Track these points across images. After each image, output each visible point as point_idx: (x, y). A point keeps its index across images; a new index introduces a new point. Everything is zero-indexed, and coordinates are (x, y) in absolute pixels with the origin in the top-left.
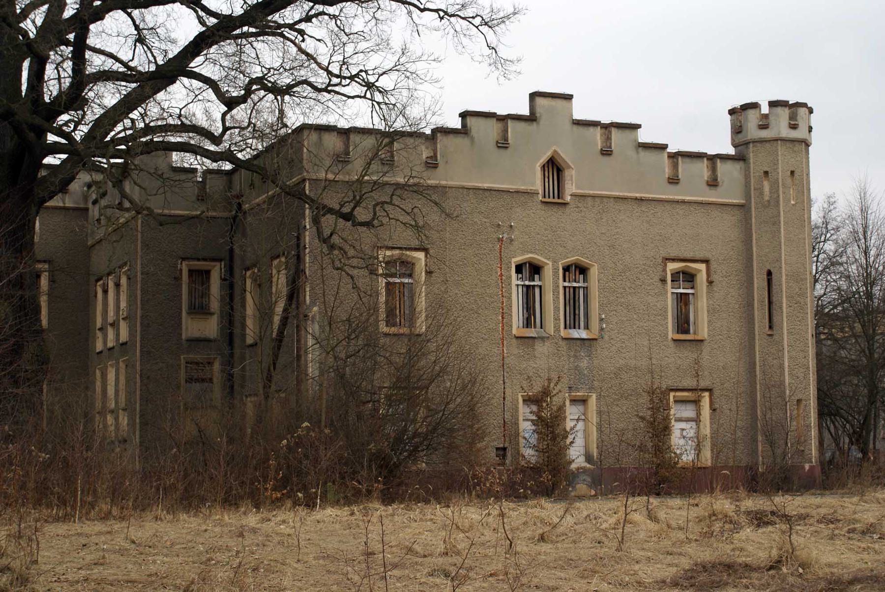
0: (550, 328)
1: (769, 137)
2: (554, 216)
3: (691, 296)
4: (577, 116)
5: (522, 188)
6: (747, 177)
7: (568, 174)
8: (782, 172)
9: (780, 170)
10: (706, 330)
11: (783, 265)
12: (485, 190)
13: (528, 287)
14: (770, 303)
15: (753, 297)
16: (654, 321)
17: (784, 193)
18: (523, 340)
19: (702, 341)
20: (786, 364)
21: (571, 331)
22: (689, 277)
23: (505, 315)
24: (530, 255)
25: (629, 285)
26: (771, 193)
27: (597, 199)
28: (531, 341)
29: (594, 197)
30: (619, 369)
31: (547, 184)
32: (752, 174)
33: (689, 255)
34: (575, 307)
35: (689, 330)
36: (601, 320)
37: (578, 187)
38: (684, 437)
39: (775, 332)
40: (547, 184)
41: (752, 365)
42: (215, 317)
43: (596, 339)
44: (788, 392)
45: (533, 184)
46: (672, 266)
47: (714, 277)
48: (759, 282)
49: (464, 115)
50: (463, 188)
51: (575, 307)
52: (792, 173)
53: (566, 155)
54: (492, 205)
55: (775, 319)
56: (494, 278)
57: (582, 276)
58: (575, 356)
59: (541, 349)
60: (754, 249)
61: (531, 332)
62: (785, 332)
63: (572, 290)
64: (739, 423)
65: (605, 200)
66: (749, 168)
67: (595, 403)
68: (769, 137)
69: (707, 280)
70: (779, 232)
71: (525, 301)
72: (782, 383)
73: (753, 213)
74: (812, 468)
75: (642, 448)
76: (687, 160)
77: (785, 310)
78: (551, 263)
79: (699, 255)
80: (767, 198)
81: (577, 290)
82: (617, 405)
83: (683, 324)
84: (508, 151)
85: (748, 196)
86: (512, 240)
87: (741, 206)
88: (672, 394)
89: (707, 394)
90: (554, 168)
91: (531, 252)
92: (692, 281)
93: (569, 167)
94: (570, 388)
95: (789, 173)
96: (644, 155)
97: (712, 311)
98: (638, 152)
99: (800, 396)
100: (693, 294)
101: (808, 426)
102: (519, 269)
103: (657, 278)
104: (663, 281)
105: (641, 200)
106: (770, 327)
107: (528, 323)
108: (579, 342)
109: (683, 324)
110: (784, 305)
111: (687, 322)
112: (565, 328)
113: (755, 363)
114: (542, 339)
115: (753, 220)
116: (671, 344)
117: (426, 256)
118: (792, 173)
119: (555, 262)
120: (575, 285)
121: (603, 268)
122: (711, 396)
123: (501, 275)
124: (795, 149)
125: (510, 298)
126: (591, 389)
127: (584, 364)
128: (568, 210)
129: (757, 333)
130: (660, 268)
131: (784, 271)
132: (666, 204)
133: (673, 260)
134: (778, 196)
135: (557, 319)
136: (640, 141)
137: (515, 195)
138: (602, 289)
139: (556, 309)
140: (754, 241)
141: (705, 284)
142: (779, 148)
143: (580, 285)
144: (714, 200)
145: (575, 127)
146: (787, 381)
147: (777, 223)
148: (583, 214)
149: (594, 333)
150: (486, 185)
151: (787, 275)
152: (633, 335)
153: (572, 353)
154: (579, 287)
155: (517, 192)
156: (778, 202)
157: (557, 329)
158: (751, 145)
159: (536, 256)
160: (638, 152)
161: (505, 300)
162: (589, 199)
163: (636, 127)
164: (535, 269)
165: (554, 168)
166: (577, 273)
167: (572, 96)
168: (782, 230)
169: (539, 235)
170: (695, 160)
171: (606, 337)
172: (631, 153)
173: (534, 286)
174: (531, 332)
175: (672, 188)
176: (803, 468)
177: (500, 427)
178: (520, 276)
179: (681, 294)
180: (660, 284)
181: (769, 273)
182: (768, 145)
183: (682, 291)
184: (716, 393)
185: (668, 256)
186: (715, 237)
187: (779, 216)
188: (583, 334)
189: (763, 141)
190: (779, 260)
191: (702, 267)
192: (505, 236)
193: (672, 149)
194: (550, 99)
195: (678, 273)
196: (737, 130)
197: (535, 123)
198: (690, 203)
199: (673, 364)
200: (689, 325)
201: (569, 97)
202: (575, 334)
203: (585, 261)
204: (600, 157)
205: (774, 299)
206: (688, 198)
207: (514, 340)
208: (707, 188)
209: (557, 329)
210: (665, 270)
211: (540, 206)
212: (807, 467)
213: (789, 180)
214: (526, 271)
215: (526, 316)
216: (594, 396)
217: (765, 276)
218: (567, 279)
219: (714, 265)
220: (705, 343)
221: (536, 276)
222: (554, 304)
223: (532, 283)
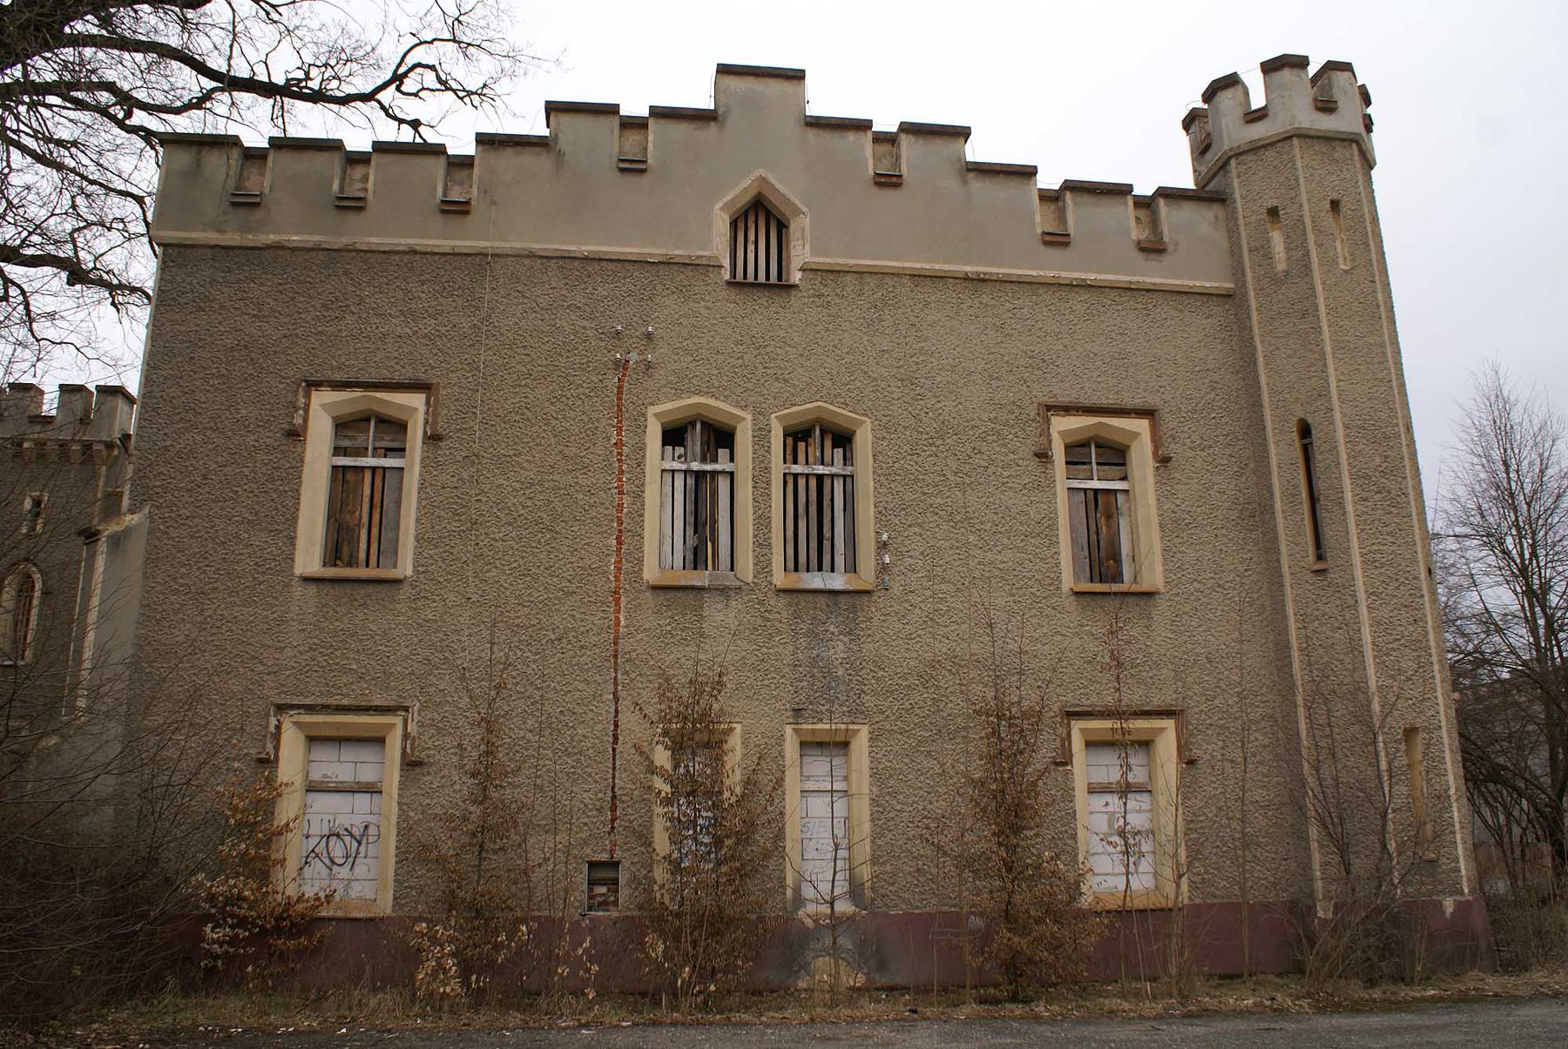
0: (747, 567)
1: (1288, 150)
2: (760, 313)
3: (1121, 498)
4: (813, 110)
5: (678, 252)
6: (1233, 233)
7: (800, 228)
8: (1308, 203)
9: (1304, 198)
10: (1159, 569)
11: (1336, 403)
12: (587, 259)
13: (699, 476)
14: (1313, 500)
15: (1270, 487)
16: (1022, 550)
17: (1319, 245)
18: (671, 594)
19: (1150, 594)
20: (1367, 636)
21: (804, 575)
22: (1115, 455)
23: (627, 536)
24: (702, 400)
26: (1288, 250)
27: (868, 279)
28: (691, 597)
29: (860, 273)
30: (934, 664)
31: (740, 254)
32: (1241, 222)
33: (1108, 400)
34: (816, 521)
35: (1121, 574)
36: (883, 546)
37: (816, 251)
39: (1330, 563)
40: (740, 254)
41: (1283, 649)
43: (868, 592)
44: (1376, 707)
45: (707, 244)
46: (1063, 425)
47: (1172, 449)
48: (1281, 450)
49: (552, 108)
50: (532, 255)
51: (816, 521)
52: (1335, 205)
53: (787, 187)
54: (602, 291)
55: (1328, 532)
57: (839, 452)
58: (812, 634)
59: (717, 614)
60: (1263, 379)
61: (701, 578)
62: (1357, 560)
63: (813, 482)
64: (1258, 794)
65: (888, 279)
66: (1234, 211)
67: (866, 750)
68: (1288, 150)
69: (1155, 454)
70: (1317, 329)
71: (690, 507)
72: (1360, 686)
73: (1253, 304)
74: (1459, 906)
75: (967, 863)
76: (1087, 199)
77: (1350, 508)
78: (749, 417)
79: (406, 374)
80: (1281, 267)
81: (827, 482)
83: (1103, 560)
84: (645, 180)
85: (1238, 272)
86: (649, 366)
87: (1227, 296)
88: (1077, 726)
89: (1169, 724)
90: (761, 216)
91: (699, 393)
92: (1124, 464)
93: (798, 212)
96: (977, 184)
97: (1171, 526)
98: (965, 183)
99: (1410, 720)
100: (1127, 491)
101: (1442, 797)
102: (673, 436)
103: (1026, 450)
104: (1043, 456)
105: (981, 280)
106: (1320, 558)
107: (697, 559)
109: (1103, 560)
110: (1348, 496)
111: (1115, 556)
112: (796, 569)
113: (1288, 647)
114: (724, 591)
115: (1255, 316)
116: (1071, 603)
117: (428, 403)
118: (1335, 205)
119: (760, 414)
120: (820, 470)
121: (885, 429)
123: (619, 444)
125: (639, 496)
126: (857, 713)
127: (837, 651)
128: (795, 300)
129: (1286, 570)
130: (1033, 428)
131: (1338, 416)
132: (1041, 290)
133: (1067, 410)
134: (1307, 254)
135: (762, 544)
136: (970, 158)
137: (662, 270)
138: (884, 476)
139: (763, 521)
140: (1261, 360)
141: (1150, 463)
142: (1297, 152)
143: (834, 470)
144: (1158, 280)
145: (811, 133)
146: (1372, 682)
147: (1308, 311)
148: (834, 310)
149: (867, 575)
150: (587, 249)
151: (1347, 427)
152: (969, 577)
153: (804, 627)
154: (832, 476)
155: (668, 263)
156: (1307, 267)
157: (763, 567)
158: (1233, 162)
159: (712, 402)
160: (965, 183)
161: (626, 500)
162: (849, 277)
163: (963, 133)
164: (721, 437)
165: (761, 216)
166: (828, 444)
168: (1324, 324)
169: (761, 374)
170: (1105, 200)
171: (896, 589)
172: (949, 182)
173: (714, 474)
174: (701, 578)
175: (1054, 254)
176: (1439, 906)
178: (679, 450)
180: (1034, 463)
181: (1305, 431)
182: (1270, 154)
183: (1096, 484)
185: (1051, 401)
186: (1169, 361)
187: (1314, 295)
188: (837, 582)
189: (1257, 148)
190: (1324, 393)
191: (1141, 426)
192: (634, 356)
193: (1048, 180)
194: (751, 79)
195: (1084, 444)
196: (1201, 150)
197: (713, 124)
198: (1099, 288)
199: (1060, 643)
200: (1118, 562)
201: (797, 76)
202: (816, 581)
203: (840, 413)
204: (875, 190)
205: (1321, 485)
206: (1091, 277)
208: (1140, 257)
209: (763, 567)
210: (1046, 432)
211: (724, 293)
212: (1449, 905)
213: (1328, 221)
214: (695, 439)
215: (691, 542)
216: (864, 732)
217: (1295, 436)
218: (801, 457)
219: (1169, 423)
220: (1158, 600)
221: (723, 453)
222: (756, 509)
223: (708, 467)
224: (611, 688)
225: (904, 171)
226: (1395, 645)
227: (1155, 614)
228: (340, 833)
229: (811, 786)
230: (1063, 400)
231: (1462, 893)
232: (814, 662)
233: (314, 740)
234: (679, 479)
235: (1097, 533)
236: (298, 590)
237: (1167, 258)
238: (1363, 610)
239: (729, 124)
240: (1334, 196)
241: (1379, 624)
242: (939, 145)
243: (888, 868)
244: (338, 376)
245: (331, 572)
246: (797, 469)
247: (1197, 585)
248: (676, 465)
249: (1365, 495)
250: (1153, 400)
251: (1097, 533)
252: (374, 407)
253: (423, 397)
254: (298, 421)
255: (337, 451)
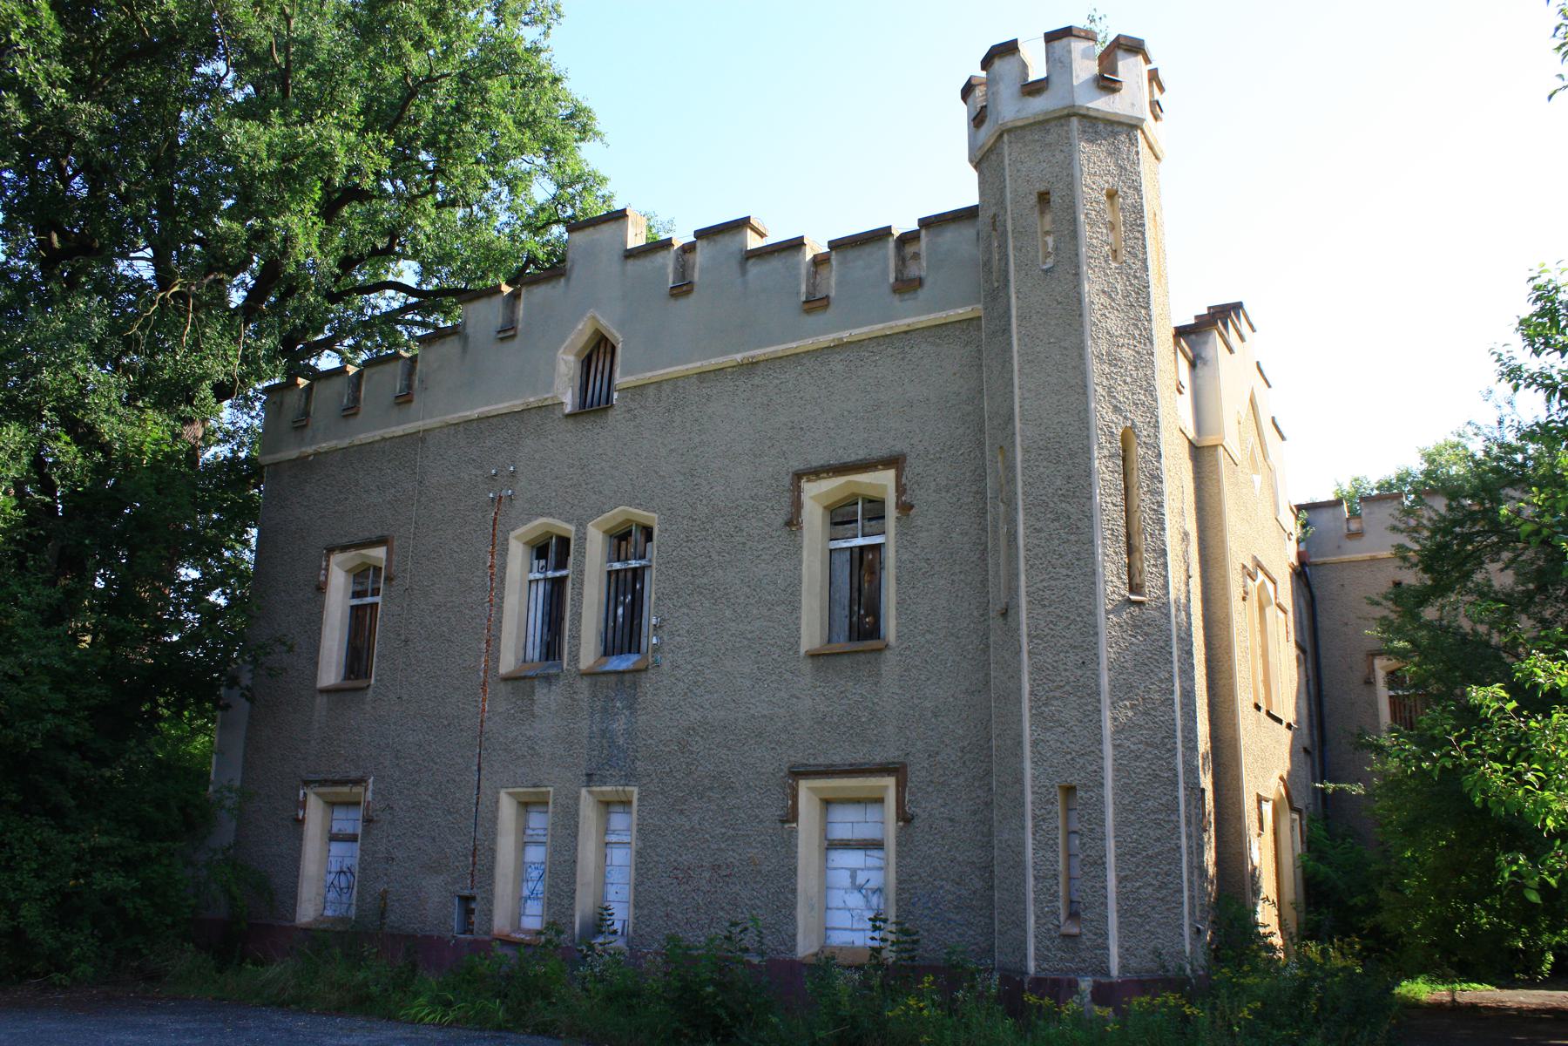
17: (1018, 249)
25: (717, 544)
33: (852, 457)
38: (860, 889)
42: (803, 650)
46: (817, 493)
56: (479, 573)
79: (879, 451)
82: (682, 812)
88: (804, 786)
94: (589, 775)
95: (1033, 199)
104: (905, 508)
108: (613, 678)
116: (806, 667)
118: (1044, 198)
122: (901, 787)
124: (1050, 138)
127: (619, 725)
133: (816, 473)
163: (743, 224)
167: (1015, 42)
171: (666, 666)
177: (466, 856)
178: (543, 562)
179: (862, 548)
184: (915, 777)
193: (816, 245)
204: (672, 301)
206: (845, 335)
207: (502, 685)
224: (476, 761)
225: (696, 277)
226: (1057, 694)
227: (884, 669)
228: (321, 871)
229: (613, 838)
230: (816, 462)
231: (1108, 974)
232: (603, 732)
233: (332, 804)
234: (541, 585)
235: (860, 591)
236: (321, 700)
237: (923, 294)
238: (1025, 656)
239: (574, 276)
240: (1042, 187)
241: (1040, 670)
242: (726, 241)
243: (646, 912)
244: (344, 541)
245: (350, 684)
246: (617, 566)
247: (928, 636)
248: (538, 576)
249: (1038, 525)
250: (899, 446)
251: (860, 591)
252: (856, 490)
253: (891, 473)
254: (322, 578)
255: (356, 595)
